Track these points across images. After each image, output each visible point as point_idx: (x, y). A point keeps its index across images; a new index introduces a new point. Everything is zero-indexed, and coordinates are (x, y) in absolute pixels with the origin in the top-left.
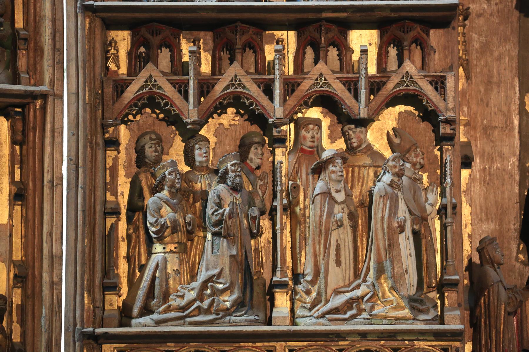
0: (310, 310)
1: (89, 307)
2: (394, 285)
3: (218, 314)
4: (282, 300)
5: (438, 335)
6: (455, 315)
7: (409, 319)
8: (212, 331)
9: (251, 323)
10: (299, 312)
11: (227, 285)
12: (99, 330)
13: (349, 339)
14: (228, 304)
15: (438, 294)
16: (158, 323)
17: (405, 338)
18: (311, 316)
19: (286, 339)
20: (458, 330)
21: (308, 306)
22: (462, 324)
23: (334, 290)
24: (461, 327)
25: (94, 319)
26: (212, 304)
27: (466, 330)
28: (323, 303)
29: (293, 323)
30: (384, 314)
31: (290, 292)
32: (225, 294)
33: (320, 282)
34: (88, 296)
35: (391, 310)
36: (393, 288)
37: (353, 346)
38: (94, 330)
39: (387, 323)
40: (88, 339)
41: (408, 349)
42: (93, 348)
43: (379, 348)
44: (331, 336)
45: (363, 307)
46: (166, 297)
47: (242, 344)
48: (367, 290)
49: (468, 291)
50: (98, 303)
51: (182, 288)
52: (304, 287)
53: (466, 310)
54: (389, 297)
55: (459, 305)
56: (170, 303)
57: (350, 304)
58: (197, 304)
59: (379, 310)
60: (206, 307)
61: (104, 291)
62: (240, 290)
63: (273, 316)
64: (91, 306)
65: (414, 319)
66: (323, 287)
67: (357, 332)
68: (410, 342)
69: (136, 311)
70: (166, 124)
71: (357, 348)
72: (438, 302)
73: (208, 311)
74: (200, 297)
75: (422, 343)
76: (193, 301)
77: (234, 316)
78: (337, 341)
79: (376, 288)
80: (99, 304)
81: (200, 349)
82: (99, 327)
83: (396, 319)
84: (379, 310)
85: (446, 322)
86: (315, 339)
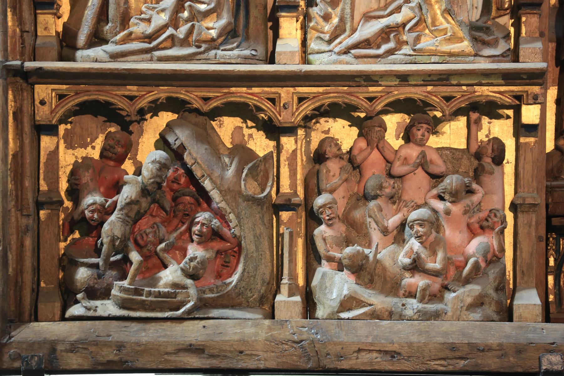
0: (330, 42)
1: (14, 31)
2: (449, 7)
3: (199, 47)
4: (290, 27)
5: (509, 77)
6: (534, 48)
7: (469, 55)
8: (190, 71)
9: (246, 60)
10: (313, 45)
11: (212, 5)
12: (29, 65)
13: (383, 83)
14: (213, 33)
15: (511, 19)
16: (114, 57)
17: (462, 82)
18: (330, 51)
19: (294, 83)
20: (538, 69)
21: (327, 37)
22: (544, 61)
23: (364, 14)
24: (543, 65)
25: (22, 48)
26: (190, 32)
27: (550, 69)
28: (347, 33)
29: (305, 61)
30: (434, 48)
31: (302, 18)
32: (209, 18)
33: (345, 3)
34: (13, 15)
35: (444, 42)
36: (448, 12)
37: (388, 93)
38: (22, 63)
39: (437, 61)
40: (15, 76)
41: (466, 97)
42: (22, 90)
43: (425, 96)
44: (357, 79)
45: (405, 38)
46: (125, 20)
47: (233, 89)
48: (411, 14)
49: (555, 15)
50: (28, 26)
51: (148, 8)
52: (321, 10)
53: (551, 41)
54: (441, 24)
55: (542, 35)
56: (131, 29)
57: (385, 34)
58: (170, 31)
59: (426, 43)
60: (182, 36)
61: (35, 9)
62: (231, 13)
63: (277, 49)
64: (18, 30)
65: (476, 55)
66: (348, 11)
67: (394, 73)
68: (469, 88)
69: (82, 39)
70: (137, 123)
71: (393, 96)
72: (512, 30)
73: (185, 42)
74: (174, 22)
75: (485, 88)
76: (164, 27)
77: (222, 50)
78: (366, 86)
79: (424, 11)
80: (29, 27)
81: (174, 95)
82: (30, 60)
83: (451, 54)
84: (426, 43)
85: (521, 59)
86: (336, 83)
